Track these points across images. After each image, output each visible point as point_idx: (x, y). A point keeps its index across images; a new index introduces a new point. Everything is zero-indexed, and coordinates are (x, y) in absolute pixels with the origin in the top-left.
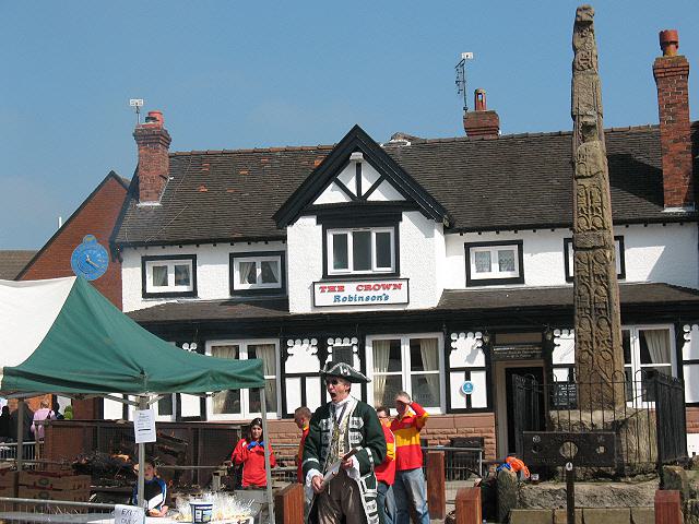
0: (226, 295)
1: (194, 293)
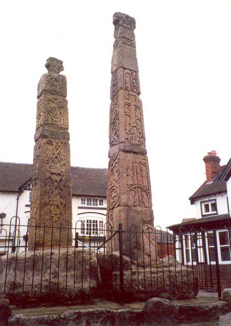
0: (201, 217)
1: (217, 214)
